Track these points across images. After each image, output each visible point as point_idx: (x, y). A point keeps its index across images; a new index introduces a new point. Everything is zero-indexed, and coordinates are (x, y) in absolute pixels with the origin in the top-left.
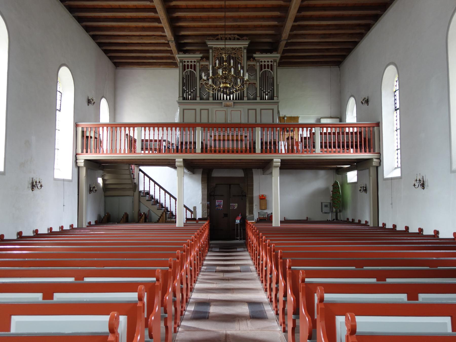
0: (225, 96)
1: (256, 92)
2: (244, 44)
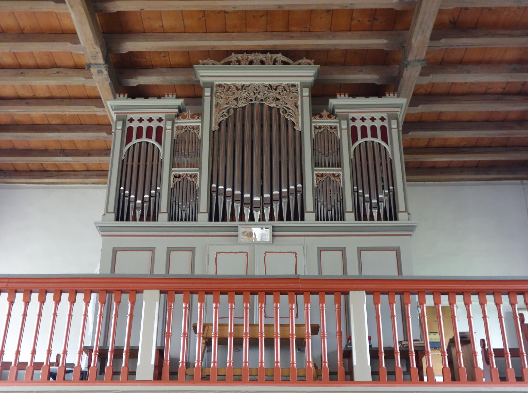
2: (304, 74)
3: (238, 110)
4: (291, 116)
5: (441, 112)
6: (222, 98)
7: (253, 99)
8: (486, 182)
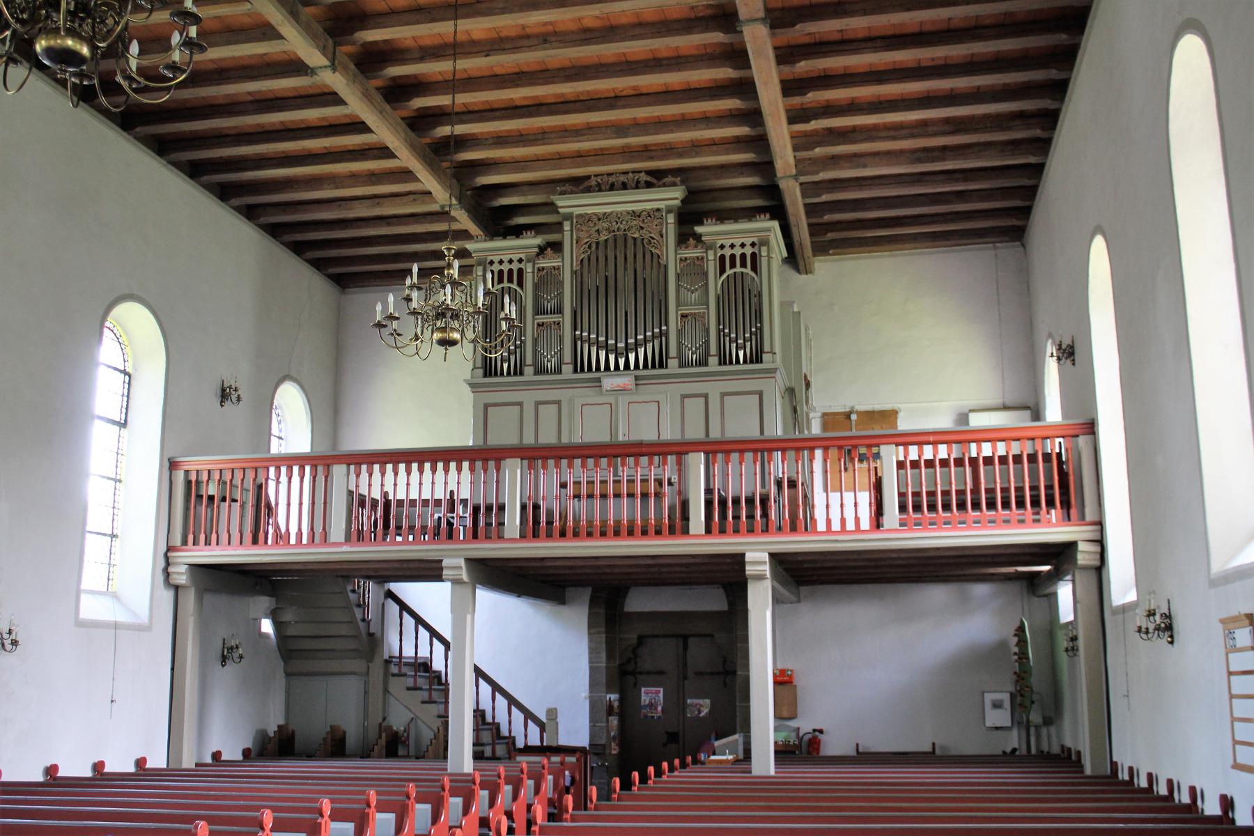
0: (612, 358)
1: (707, 342)
2: (672, 196)
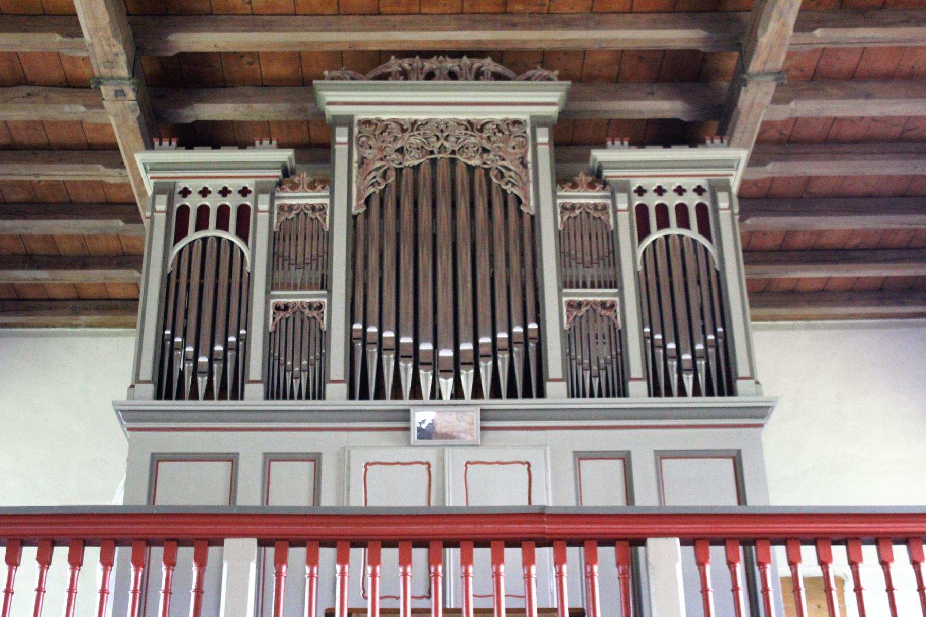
2: (542, 99)
3: (404, 171)
4: (514, 185)
5: (810, 178)
6: (371, 147)
7: (436, 151)
8: (880, 321)
